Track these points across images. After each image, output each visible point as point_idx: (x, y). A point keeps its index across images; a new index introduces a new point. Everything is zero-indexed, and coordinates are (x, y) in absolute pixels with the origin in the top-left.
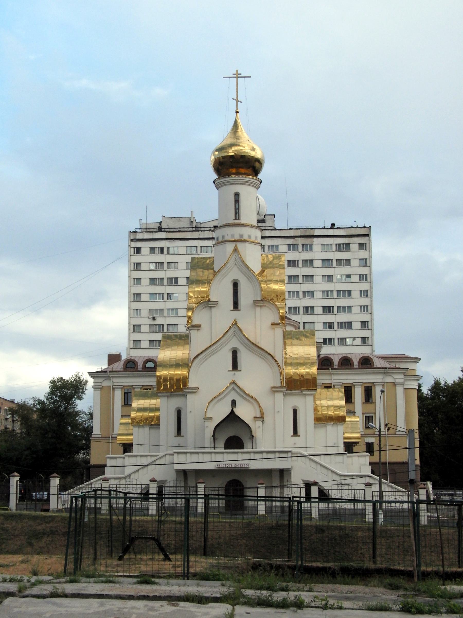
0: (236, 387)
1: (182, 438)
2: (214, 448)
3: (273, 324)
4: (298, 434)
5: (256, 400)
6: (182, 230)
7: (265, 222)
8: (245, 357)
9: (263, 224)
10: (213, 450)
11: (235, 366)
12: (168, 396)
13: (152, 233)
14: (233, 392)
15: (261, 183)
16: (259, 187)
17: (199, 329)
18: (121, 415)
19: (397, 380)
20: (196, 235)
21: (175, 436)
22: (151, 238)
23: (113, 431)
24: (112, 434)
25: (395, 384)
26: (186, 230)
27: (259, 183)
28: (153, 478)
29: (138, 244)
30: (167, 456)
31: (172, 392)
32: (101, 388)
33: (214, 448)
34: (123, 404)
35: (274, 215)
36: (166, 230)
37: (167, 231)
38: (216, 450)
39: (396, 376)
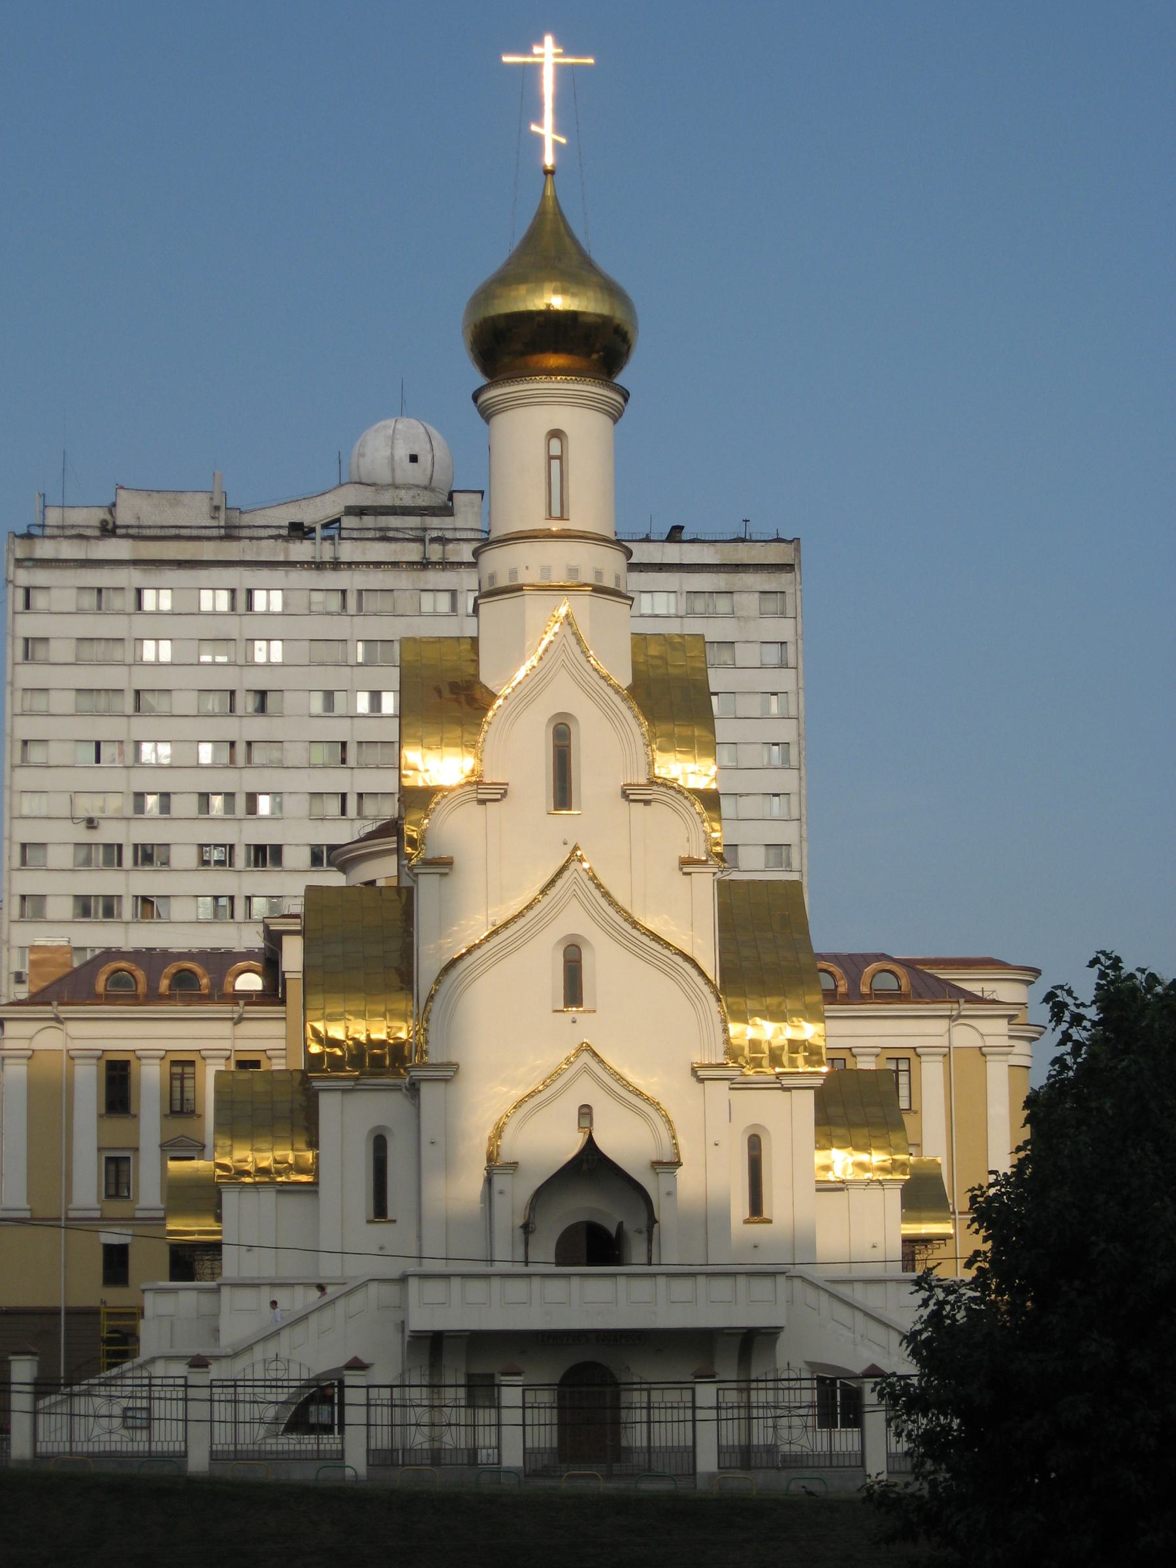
0: (593, 1064)
1: (626, 1226)
2: (527, 1263)
3: (686, 862)
4: (766, 1214)
5: (656, 1105)
6: (184, 532)
7: (452, 515)
8: (606, 963)
9: (447, 522)
10: (520, 1269)
11: (573, 993)
12: (344, 1091)
13: (84, 543)
14: (585, 1082)
15: (626, 400)
16: (621, 415)
17: (446, 874)
18: (95, 1146)
19: (990, 1041)
20: (231, 550)
21: (369, 1222)
22: (83, 557)
23: (69, 1199)
24: (67, 1210)
25: (982, 1052)
26: (195, 532)
27: (620, 399)
28: (356, 1359)
29: (40, 577)
30: (373, 1288)
31: (357, 1078)
32: (30, 1058)
33: (527, 1263)
34: (168, 1111)
35: (482, 493)
36: (132, 531)
37: (138, 535)
38: (532, 1269)
39: (985, 1026)
